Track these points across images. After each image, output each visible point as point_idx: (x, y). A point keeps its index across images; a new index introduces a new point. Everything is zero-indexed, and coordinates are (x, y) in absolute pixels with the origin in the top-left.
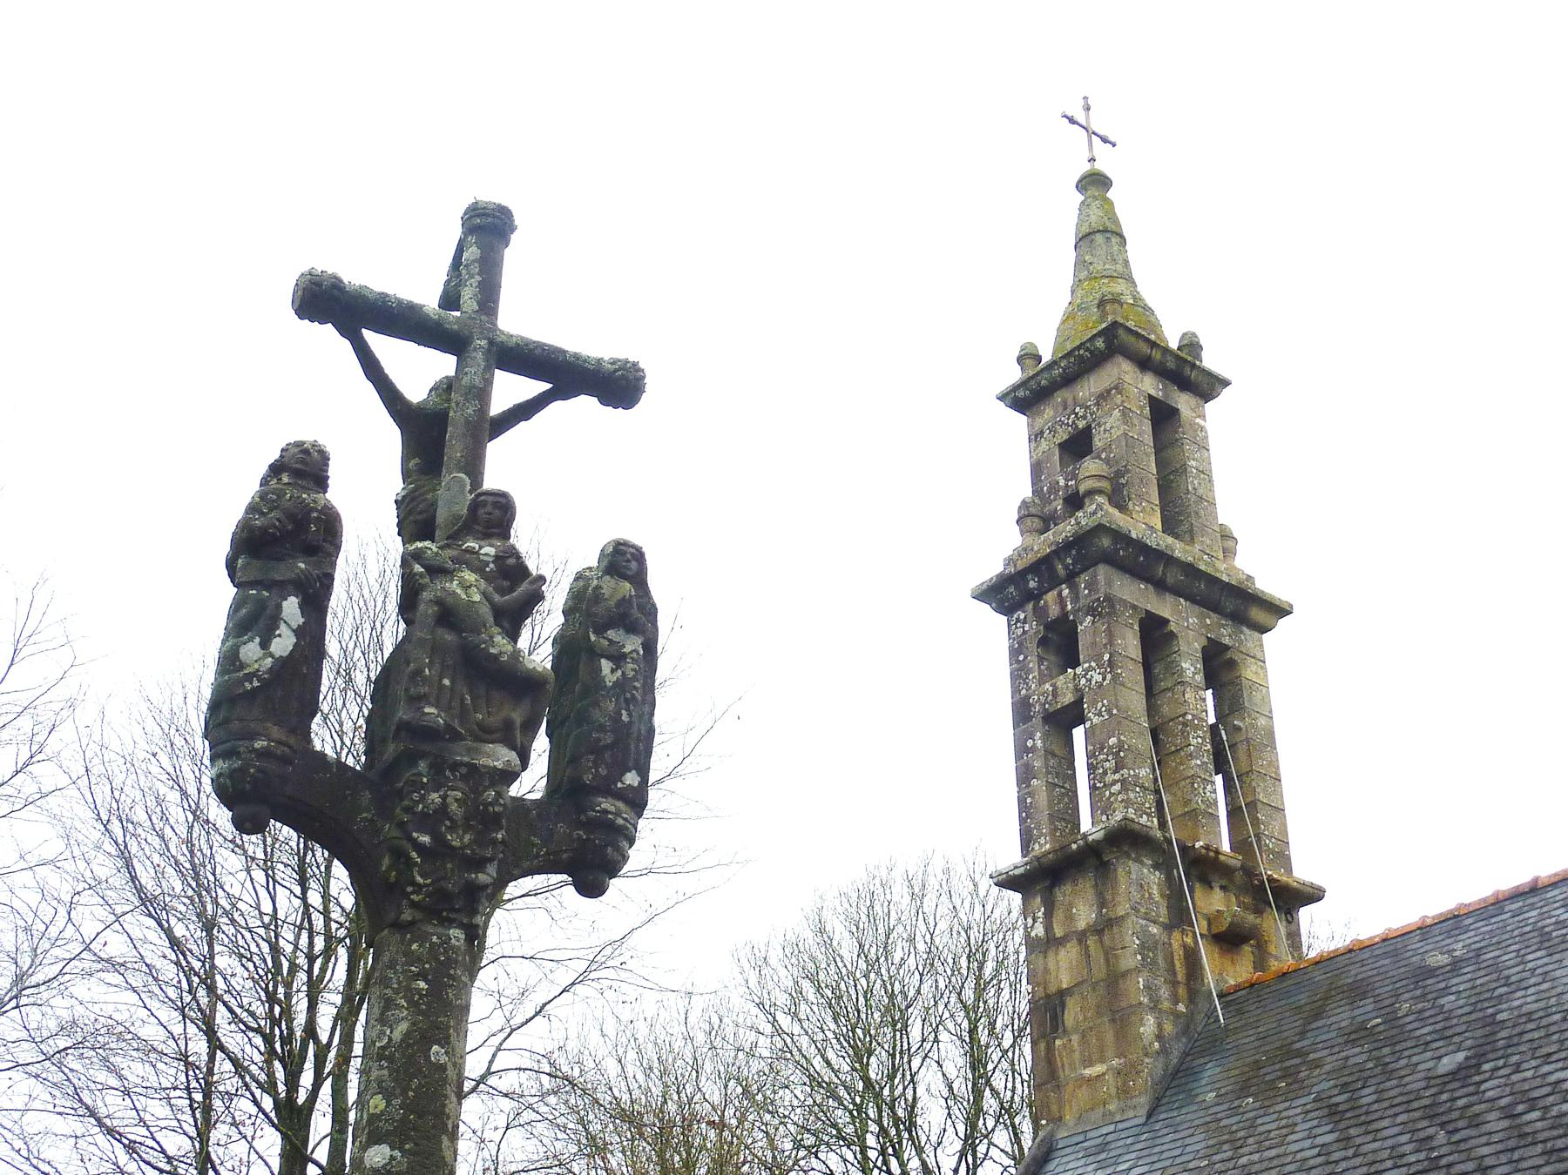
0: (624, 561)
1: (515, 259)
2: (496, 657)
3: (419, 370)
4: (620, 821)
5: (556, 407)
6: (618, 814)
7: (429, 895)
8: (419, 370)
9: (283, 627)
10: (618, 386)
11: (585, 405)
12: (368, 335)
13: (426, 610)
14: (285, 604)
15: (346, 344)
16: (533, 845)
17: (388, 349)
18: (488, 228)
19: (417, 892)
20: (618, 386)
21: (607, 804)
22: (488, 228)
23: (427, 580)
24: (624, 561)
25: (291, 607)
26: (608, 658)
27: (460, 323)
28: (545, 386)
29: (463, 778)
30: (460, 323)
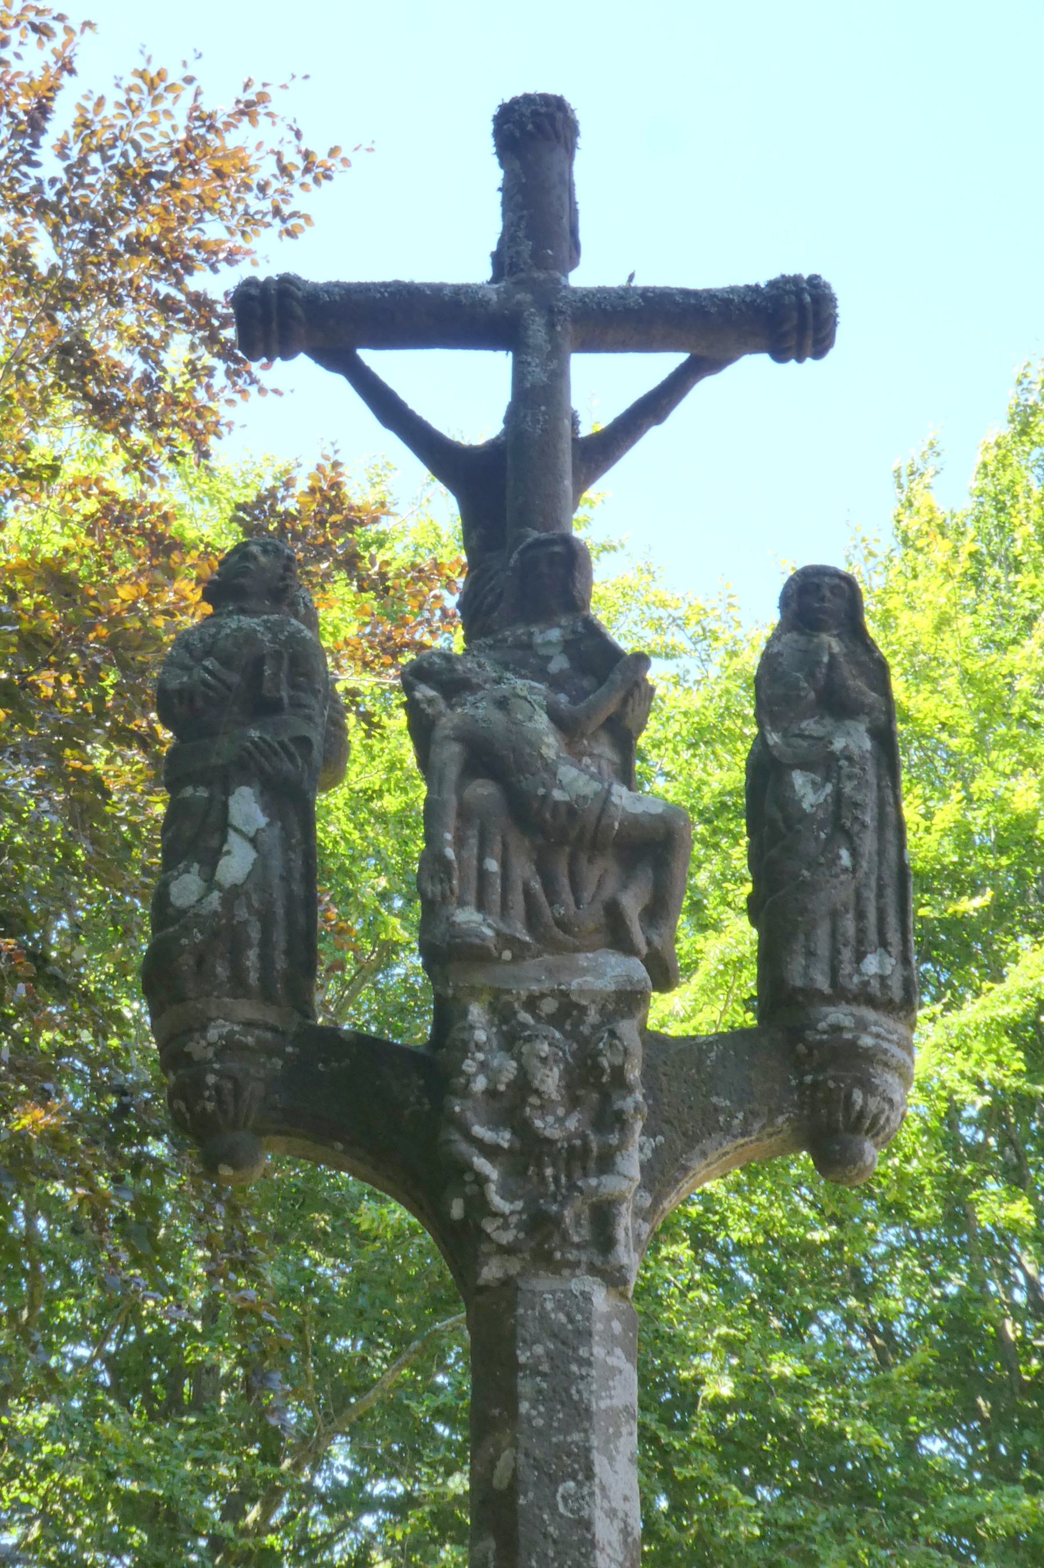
0: (822, 603)
1: (595, 177)
2: (571, 811)
3: (467, 392)
4: (867, 1041)
5: (706, 390)
6: (862, 1025)
7: (519, 1227)
8: (467, 392)
9: (233, 837)
10: (791, 319)
11: (753, 368)
12: (368, 356)
13: (450, 754)
14: (232, 801)
15: (339, 384)
16: (717, 1109)
17: (408, 371)
18: (534, 137)
19: (505, 1227)
20: (791, 319)
21: (839, 1015)
22: (534, 137)
23: (442, 705)
24: (822, 603)
25: (246, 807)
26: (805, 766)
27: (529, 299)
28: (679, 358)
29: (555, 1021)
30: (529, 299)
